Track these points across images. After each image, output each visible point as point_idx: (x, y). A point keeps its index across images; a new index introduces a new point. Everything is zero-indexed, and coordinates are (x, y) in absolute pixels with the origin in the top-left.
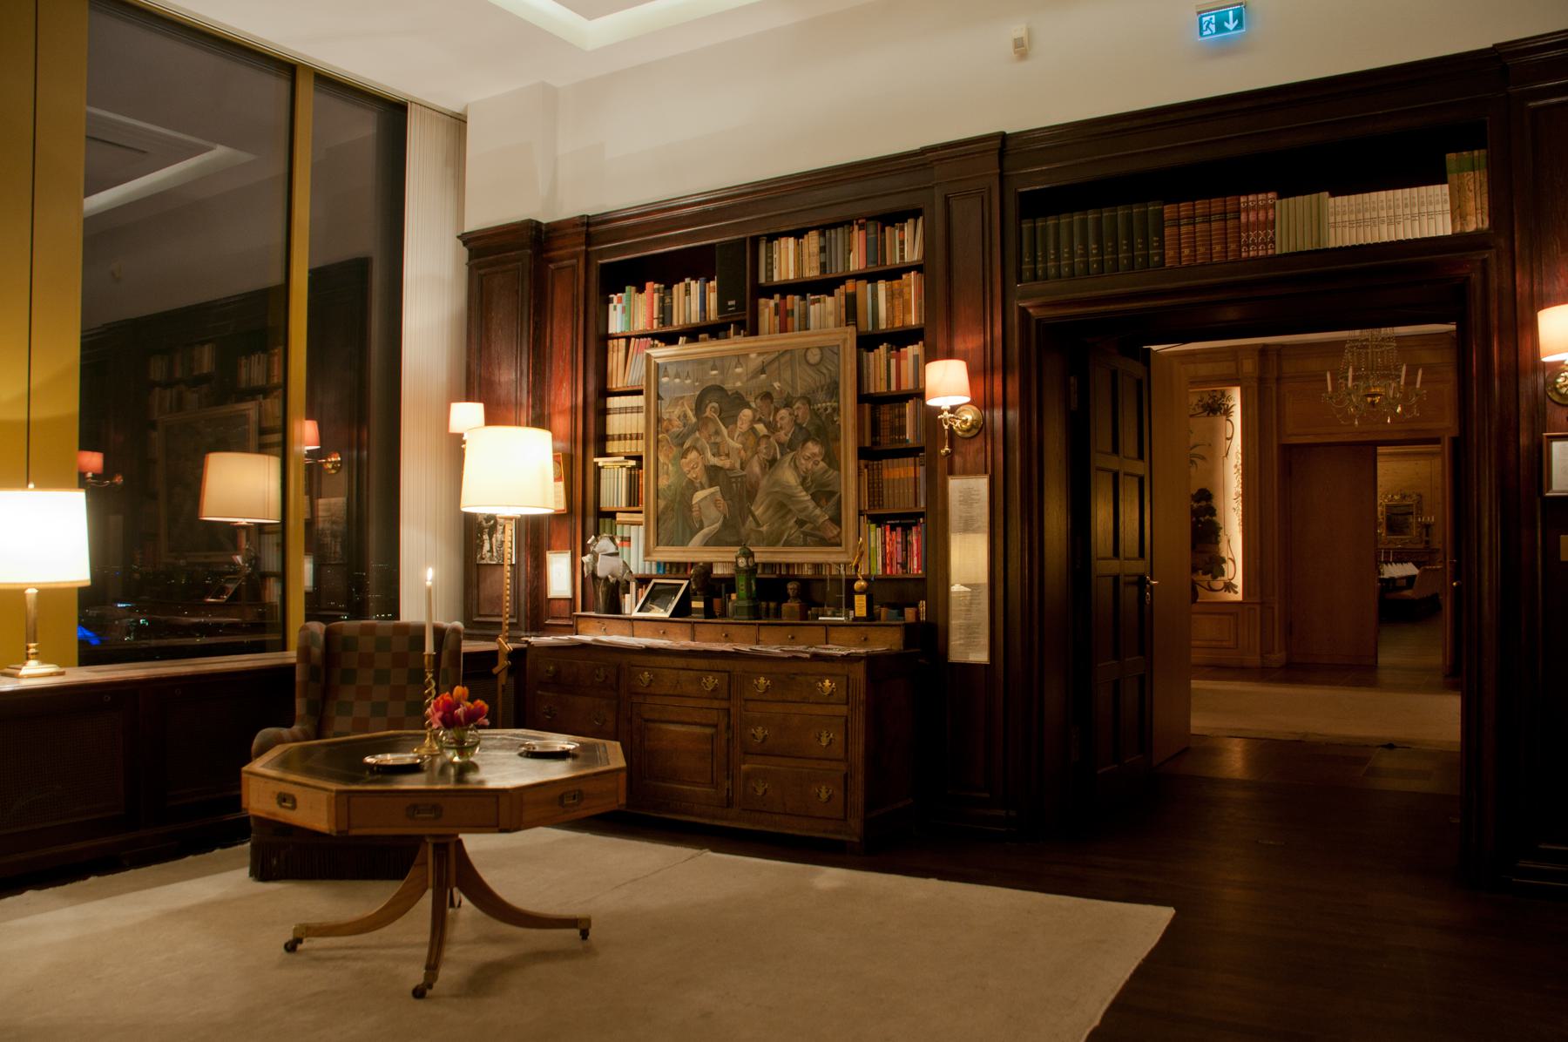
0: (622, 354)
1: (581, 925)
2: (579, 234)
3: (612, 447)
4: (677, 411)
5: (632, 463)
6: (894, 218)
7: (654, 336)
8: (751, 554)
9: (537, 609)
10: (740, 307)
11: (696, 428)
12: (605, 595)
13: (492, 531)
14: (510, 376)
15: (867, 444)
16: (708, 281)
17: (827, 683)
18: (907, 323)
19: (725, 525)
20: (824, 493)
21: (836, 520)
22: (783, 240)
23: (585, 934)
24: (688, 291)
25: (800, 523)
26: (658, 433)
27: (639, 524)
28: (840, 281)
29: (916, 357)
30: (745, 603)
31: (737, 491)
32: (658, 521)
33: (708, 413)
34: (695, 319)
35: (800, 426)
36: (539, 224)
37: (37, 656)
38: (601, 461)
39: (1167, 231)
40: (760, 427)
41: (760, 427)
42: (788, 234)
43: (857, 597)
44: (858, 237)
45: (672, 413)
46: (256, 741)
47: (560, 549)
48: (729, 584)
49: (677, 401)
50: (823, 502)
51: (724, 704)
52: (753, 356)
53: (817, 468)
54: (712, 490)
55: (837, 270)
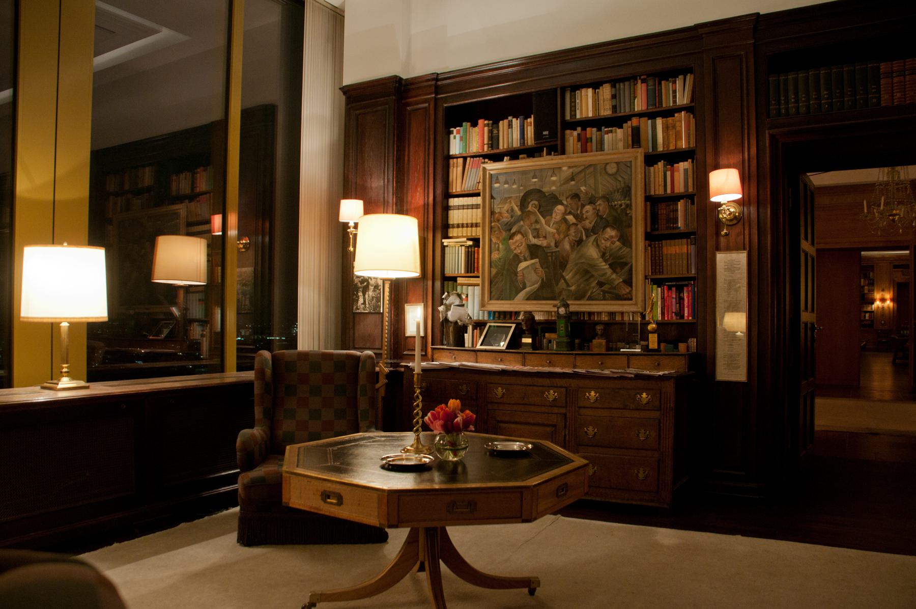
0: (460, 169)
1: (529, 584)
2: (430, 86)
3: (452, 232)
4: (506, 207)
5: (470, 243)
6: (670, 75)
7: (485, 156)
8: (566, 306)
9: (399, 343)
10: (553, 135)
11: (521, 218)
12: (449, 333)
13: (365, 290)
14: (378, 183)
15: (649, 230)
16: (526, 118)
17: (644, 395)
18: (679, 146)
19: (543, 285)
20: (619, 263)
21: (629, 282)
22: (584, 90)
23: (532, 592)
24: (510, 125)
25: (601, 284)
26: (491, 222)
27: (478, 285)
28: (628, 118)
29: (686, 171)
30: (565, 340)
31: (553, 263)
32: (491, 282)
33: (530, 208)
34: (516, 144)
35: (601, 217)
36: (401, 79)
37: (68, 374)
38: (446, 242)
39: (883, 81)
40: (570, 218)
41: (570, 218)
42: (587, 86)
43: (650, 335)
44: (641, 89)
45: (502, 208)
46: (239, 440)
47: (416, 302)
48: (549, 326)
49: (506, 200)
50: (618, 270)
51: (563, 411)
52: (565, 168)
53: (614, 246)
54: (533, 261)
55: (625, 110)
